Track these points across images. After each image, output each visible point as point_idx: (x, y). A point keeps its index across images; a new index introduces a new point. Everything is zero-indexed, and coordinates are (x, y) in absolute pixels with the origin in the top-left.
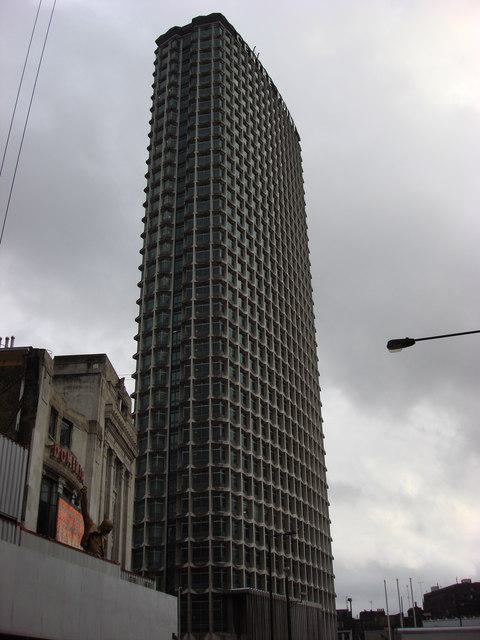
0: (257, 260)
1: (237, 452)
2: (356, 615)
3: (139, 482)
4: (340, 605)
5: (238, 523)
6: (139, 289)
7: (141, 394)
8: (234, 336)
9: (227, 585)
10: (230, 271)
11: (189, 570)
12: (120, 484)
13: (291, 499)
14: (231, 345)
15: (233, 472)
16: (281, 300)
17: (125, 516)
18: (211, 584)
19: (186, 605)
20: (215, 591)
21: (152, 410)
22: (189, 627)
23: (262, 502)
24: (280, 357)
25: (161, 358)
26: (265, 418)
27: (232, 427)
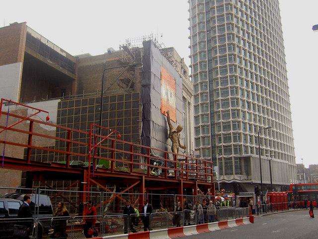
0: (250, 8)
1: (243, 90)
2: (307, 167)
3: (196, 107)
4: (298, 161)
5: (246, 135)
6: (189, 21)
7: (194, 66)
8: (237, 22)
9: (241, 154)
10: (235, 7)
11: (223, 159)
12: (186, 108)
13: (271, 111)
14: (238, 46)
15: (242, 111)
16: (262, 10)
17: (190, 123)
18: (233, 152)
19: (222, 162)
20: (235, 144)
21: (199, 52)
22: (224, 172)
23: (257, 113)
24: (263, 40)
25: (201, 36)
26: (256, 122)
27: (242, 111)
